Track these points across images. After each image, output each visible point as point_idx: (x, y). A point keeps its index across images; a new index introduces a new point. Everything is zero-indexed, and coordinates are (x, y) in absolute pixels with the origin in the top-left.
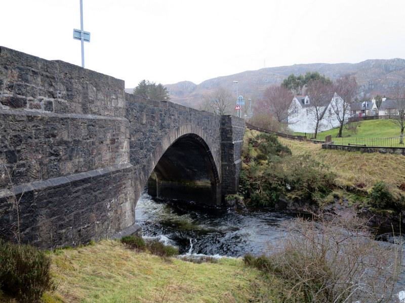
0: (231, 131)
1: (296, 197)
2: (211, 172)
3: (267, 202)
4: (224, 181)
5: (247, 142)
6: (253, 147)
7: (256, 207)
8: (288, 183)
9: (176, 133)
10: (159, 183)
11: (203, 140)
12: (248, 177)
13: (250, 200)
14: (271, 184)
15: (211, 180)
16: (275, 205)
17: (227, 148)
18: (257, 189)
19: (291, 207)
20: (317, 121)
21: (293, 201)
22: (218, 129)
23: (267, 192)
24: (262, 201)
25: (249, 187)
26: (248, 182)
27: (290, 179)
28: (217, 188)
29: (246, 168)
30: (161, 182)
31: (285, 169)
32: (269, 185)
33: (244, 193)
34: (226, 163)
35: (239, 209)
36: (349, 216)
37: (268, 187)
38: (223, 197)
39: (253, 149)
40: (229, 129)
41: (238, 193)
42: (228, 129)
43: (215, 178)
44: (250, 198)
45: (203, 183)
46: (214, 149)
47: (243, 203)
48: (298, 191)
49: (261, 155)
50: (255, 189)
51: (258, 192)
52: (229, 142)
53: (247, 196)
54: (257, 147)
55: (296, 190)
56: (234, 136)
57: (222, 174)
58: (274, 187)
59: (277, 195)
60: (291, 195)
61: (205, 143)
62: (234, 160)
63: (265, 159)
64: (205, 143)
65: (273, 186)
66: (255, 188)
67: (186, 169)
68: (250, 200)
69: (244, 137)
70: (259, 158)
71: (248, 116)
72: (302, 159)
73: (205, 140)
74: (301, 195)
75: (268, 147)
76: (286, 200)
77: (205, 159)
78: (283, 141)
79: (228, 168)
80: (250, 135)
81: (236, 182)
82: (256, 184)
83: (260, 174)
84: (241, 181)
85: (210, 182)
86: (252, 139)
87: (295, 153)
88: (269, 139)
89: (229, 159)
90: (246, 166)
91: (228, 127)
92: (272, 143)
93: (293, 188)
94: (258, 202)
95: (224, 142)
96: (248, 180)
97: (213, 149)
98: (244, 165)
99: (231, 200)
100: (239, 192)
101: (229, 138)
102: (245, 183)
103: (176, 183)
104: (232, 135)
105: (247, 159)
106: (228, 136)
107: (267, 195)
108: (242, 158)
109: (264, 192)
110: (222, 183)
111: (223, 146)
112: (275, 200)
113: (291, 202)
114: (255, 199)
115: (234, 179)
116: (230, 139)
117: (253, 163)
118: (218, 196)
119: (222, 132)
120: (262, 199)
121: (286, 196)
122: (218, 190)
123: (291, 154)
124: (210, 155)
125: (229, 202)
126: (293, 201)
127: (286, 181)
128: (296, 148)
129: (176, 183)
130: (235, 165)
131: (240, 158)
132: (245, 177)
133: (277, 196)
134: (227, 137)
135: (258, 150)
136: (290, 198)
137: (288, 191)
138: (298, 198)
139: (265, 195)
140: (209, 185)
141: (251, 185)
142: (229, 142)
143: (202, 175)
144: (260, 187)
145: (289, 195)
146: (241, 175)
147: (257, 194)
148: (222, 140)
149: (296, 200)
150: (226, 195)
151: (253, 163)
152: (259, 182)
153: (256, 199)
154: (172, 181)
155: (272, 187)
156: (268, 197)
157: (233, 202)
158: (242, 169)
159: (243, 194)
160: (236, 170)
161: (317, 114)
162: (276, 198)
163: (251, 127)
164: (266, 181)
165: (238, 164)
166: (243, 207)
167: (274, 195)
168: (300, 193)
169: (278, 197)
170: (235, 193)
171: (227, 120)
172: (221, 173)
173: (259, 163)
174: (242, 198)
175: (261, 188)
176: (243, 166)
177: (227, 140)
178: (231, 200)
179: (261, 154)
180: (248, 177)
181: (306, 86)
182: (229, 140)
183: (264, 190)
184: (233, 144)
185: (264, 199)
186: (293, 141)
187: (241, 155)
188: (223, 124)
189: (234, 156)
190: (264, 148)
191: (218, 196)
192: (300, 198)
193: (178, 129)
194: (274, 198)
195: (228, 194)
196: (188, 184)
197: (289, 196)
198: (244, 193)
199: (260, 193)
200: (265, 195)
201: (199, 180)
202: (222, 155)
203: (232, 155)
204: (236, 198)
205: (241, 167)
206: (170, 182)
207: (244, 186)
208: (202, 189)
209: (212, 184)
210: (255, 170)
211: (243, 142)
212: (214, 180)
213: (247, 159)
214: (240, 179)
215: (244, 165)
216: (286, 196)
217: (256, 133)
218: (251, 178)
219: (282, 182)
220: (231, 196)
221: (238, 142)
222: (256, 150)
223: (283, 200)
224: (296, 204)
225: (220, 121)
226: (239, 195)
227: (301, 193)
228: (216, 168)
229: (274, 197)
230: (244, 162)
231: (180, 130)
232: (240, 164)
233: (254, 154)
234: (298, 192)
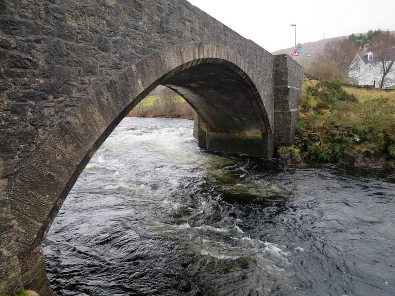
0: (286, 73)
1: (367, 151)
2: (261, 120)
3: (329, 156)
4: (277, 131)
5: (305, 91)
6: (313, 95)
7: (314, 161)
8: (357, 134)
9: (197, 51)
10: (208, 135)
11: (247, 77)
12: (306, 128)
13: (307, 153)
14: (333, 135)
15: (261, 130)
16: (338, 159)
17: (281, 93)
18: (316, 140)
19: (361, 162)
20: (382, 75)
21: (363, 156)
22: (270, 69)
23: (328, 145)
24: (323, 154)
25: (307, 138)
26: (305, 133)
27: (361, 128)
28: (269, 139)
29: (303, 118)
30: (210, 134)
31: (354, 118)
32: (331, 137)
33: (300, 145)
34: (280, 111)
35: (295, 162)
36: (164, 170)
37: (331, 138)
38: (276, 149)
39: (312, 98)
40: (284, 70)
41: (293, 145)
42: (282, 71)
43: (266, 127)
44: (307, 151)
45: (253, 133)
46: (265, 92)
47: (299, 157)
48: (370, 143)
49: (321, 104)
50: (314, 141)
51: (317, 144)
52: (283, 86)
53: (304, 149)
54: (317, 95)
55: (368, 142)
56: (290, 80)
57: (275, 124)
58: (339, 139)
59: (341, 148)
60: (360, 148)
61: (251, 82)
62: (290, 107)
63: (327, 108)
64: (251, 82)
65: (338, 137)
66: (314, 140)
67: (234, 118)
68: (307, 153)
69: (300, 86)
70: (319, 108)
71: (307, 67)
72: (376, 103)
73: (250, 77)
74: (374, 148)
75: (330, 95)
76: (354, 154)
77: (253, 104)
78: (349, 91)
79: (282, 116)
80: (308, 84)
81: (291, 132)
82: (316, 135)
83: (321, 124)
84: (297, 133)
85: (260, 132)
86: (312, 88)
87: (362, 101)
88: (329, 86)
89: (283, 106)
90: (304, 116)
91: (283, 69)
92: (335, 91)
93: (363, 140)
94: (317, 156)
95: (277, 86)
96: (306, 132)
97: (262, 91)
98: (302, 115)
99: (285, 153)
100: (295, 144)
101: (283, 81)
102: (301, 134)
103: (225, 135)
104: (287, 77)
105: (305, 108)
106: (283, 79)
107: (329, 148)
108: (300, 107)
109: (325, 145)
110: (275, 134)
111: (276, 91)
112: (339, 154)
113: (361, 156)
114: (313, 152)
115: (289, 129)
116: (285, 83)
117: (312, 113)
118: (270, 148)
119: (275, 75)
120: (321, 153)
121: (354, 149)
122: (270, 142)
123: (357, 101)
124: (258, 98)
125: (282, 155)
126: (363, 156)
127: (355, 131)
128: (362, 96)
129: (225, 135)
130: (290, 112)
131: (297, 107)
132: (303, 128)
133: (342, 149)
134: (281, 81)
135: (318, 99)
136: (359, 151)
137: (356, 143)
138: (370, 152)
139: (327, 148)
140: (260, 136)
141: (309, 136)
142: (283, 86)
143: (252, 124)
144: (320, 138)
145: (358, 148)
146: (298, 126)
147: (316, 146)
148: (276, 84)
149: (367, 154)
150: (279, 148)
151: (312, 113)
152: (318, 134)
153: (315, 152)
154: (220, 132)
155: (335, 138)
156: (329, 150)
157: (287, 155)
158: (299, 120)
159: (299, 147)
160: (292, 119)
161: (384, 67)
162: (340, 151)
163: (311, 78)
164: (327, 132)
165: (294, 112)
166: (298, 161)
167: (337, 148)
168: (372, 145)
169: (343, 150)
170: (289, 145)
171: (281, 60)
172: (273, 122)
173: (319, 113)
174: (297, 151)
175: (321, 140)
176: (300, 116)
177: (281, 84)
178: (285, 153)
179: (322, 102)
180: (306, 128)
181: (366, 47)
182: (284, 85)
183: (325, 142)
184: (289, 89)
185: (325, 152)
186: (359, 90)
187: (299, 104)
188: (276, 65)
189: (290, 102)
190: (324, 96)
191: (270, 148)
192: (372, 152)
193: (200, 45)
194: (338, 151)
195: (281, 146)
196: (237, 134)
197: (357, 149)
198: (300, 145)
199: (321, 146)
200: (327, 148)
201: (249, 130)
202: (275, 102)
203: (287, 102)
204: (290, 151)
205: (298, 117)
206: (219, 133)
207: (301, 138)
208: (252, 140)
209: (263, 134)
210: (315, 118)
211: (301, 91)
212: (264, 130)
213: (305, 108)
214: (296, 130)
215: (302, 115)
216: (354, 149)
217: (314, 83)
218: (309, 129)
219: (349, 132)
220: (284, 148)
221: (294, 88)
222: (315, 99)
223: (350, 154)
224: (367, 159)
225: (272, 62)
226: (295, 147)
227: (375, 146)
228: (267, 115)
229: (337, 150)
230: (302, 112)
231: (205, 49)
232: (297, 113)
233: (313, 103)
234: (370, 145)
